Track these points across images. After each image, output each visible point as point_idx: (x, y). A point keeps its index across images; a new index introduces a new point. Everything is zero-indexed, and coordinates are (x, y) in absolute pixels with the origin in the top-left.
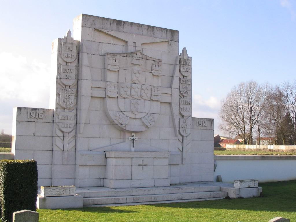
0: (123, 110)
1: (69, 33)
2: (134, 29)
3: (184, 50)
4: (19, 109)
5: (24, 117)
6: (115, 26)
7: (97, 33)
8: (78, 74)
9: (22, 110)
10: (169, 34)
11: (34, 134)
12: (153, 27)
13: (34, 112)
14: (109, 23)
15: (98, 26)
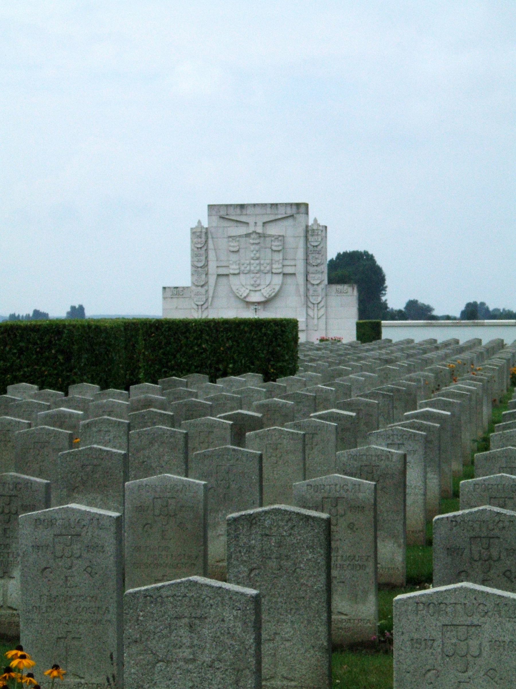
0: (244, 284)
1: (199, 222)
2: (258, 210)
3: (315, 220)
4: (164, 288)
5: (169, 294)
6: (238, 211)
7: (222, 220)
8: (207, 258)
9: (167, 290)
10: (294, 208)
11: (176, 308)
12: (277, 205)
13: (175, 290)
14: (232, 208)
15: (223, 213)
